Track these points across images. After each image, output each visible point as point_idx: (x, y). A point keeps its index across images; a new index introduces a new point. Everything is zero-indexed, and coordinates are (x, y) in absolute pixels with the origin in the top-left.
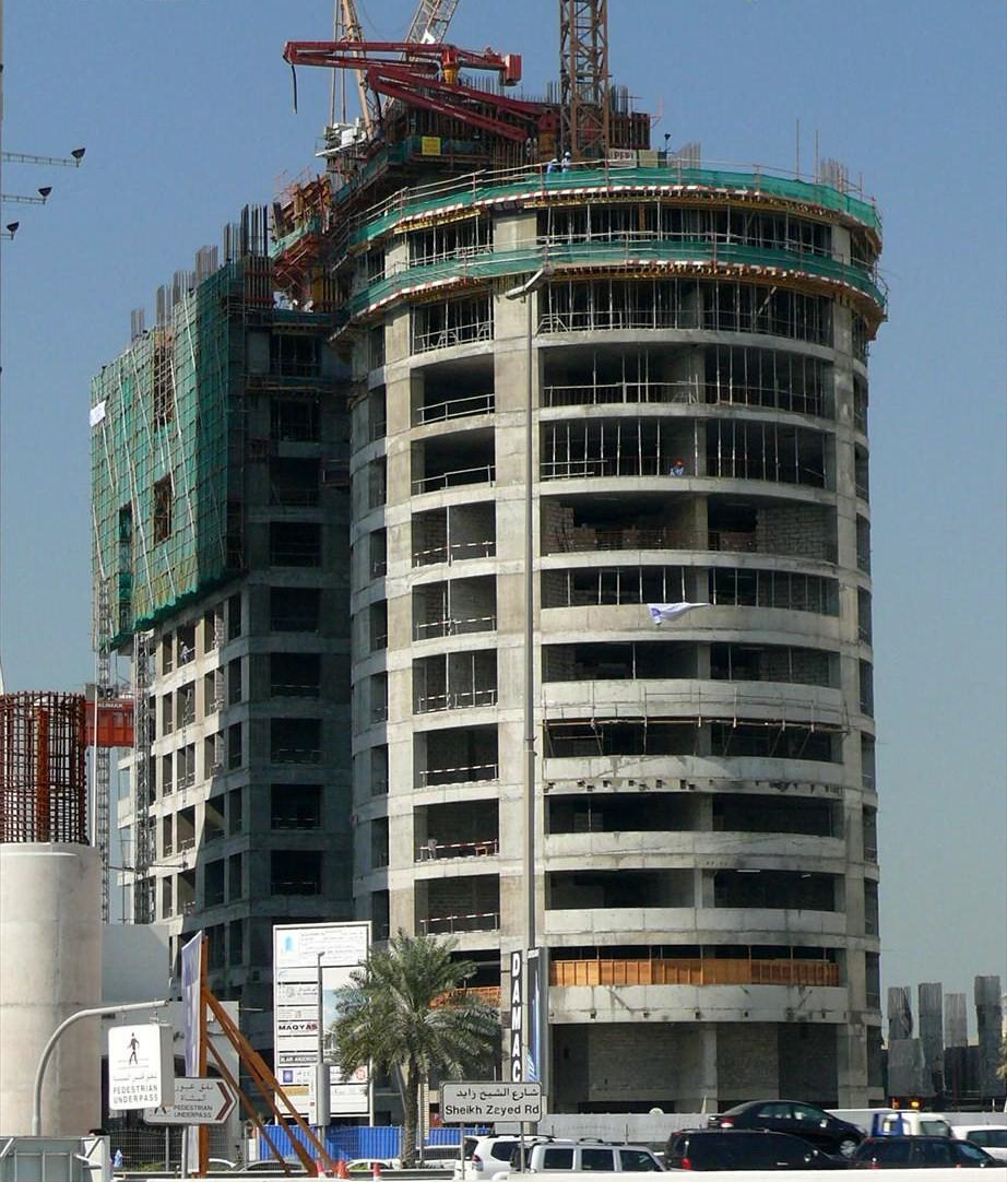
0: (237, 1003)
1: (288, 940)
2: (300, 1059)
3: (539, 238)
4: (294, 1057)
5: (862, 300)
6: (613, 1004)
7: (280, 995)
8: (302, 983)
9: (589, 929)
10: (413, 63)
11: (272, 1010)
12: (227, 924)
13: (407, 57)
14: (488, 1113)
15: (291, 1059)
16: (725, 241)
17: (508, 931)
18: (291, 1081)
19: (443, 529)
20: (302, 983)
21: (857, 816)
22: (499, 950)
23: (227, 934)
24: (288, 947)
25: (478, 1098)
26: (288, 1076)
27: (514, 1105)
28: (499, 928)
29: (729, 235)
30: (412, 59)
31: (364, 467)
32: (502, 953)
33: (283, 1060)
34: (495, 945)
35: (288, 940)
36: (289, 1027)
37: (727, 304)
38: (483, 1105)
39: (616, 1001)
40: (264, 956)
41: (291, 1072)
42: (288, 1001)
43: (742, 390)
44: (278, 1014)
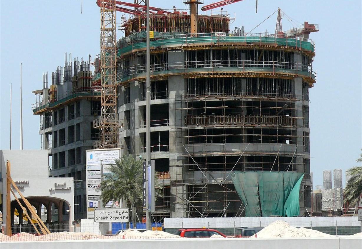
0: (73, 178)
1: (91, 155)
2: (95, 198)
4: (93, 198)
5: (305, 177)
6: (210, 178)
7: (88, 175)
8: (96, 171)
9: (201, 151)
11: (86, 180)
12: (76, 149)
14: (110, 219)
15: (92, 198)
17: (172, 151)
18: (92, 206)
20: (96, 171)
21: (301, 109)
22: (169, 158)
23: (76, 152)
24: (91, 158)
25: (107, 214)
26: (91, 204)
27: (120, 216)
28: (169, 150)
32: (170, 159)
33: (89, 198)
35: (91, 155)
37: (306, 71)
38: (109, 216)
39: (211, 177)
40: (82, 160)
41: (92, 203)
44: (88, 182)
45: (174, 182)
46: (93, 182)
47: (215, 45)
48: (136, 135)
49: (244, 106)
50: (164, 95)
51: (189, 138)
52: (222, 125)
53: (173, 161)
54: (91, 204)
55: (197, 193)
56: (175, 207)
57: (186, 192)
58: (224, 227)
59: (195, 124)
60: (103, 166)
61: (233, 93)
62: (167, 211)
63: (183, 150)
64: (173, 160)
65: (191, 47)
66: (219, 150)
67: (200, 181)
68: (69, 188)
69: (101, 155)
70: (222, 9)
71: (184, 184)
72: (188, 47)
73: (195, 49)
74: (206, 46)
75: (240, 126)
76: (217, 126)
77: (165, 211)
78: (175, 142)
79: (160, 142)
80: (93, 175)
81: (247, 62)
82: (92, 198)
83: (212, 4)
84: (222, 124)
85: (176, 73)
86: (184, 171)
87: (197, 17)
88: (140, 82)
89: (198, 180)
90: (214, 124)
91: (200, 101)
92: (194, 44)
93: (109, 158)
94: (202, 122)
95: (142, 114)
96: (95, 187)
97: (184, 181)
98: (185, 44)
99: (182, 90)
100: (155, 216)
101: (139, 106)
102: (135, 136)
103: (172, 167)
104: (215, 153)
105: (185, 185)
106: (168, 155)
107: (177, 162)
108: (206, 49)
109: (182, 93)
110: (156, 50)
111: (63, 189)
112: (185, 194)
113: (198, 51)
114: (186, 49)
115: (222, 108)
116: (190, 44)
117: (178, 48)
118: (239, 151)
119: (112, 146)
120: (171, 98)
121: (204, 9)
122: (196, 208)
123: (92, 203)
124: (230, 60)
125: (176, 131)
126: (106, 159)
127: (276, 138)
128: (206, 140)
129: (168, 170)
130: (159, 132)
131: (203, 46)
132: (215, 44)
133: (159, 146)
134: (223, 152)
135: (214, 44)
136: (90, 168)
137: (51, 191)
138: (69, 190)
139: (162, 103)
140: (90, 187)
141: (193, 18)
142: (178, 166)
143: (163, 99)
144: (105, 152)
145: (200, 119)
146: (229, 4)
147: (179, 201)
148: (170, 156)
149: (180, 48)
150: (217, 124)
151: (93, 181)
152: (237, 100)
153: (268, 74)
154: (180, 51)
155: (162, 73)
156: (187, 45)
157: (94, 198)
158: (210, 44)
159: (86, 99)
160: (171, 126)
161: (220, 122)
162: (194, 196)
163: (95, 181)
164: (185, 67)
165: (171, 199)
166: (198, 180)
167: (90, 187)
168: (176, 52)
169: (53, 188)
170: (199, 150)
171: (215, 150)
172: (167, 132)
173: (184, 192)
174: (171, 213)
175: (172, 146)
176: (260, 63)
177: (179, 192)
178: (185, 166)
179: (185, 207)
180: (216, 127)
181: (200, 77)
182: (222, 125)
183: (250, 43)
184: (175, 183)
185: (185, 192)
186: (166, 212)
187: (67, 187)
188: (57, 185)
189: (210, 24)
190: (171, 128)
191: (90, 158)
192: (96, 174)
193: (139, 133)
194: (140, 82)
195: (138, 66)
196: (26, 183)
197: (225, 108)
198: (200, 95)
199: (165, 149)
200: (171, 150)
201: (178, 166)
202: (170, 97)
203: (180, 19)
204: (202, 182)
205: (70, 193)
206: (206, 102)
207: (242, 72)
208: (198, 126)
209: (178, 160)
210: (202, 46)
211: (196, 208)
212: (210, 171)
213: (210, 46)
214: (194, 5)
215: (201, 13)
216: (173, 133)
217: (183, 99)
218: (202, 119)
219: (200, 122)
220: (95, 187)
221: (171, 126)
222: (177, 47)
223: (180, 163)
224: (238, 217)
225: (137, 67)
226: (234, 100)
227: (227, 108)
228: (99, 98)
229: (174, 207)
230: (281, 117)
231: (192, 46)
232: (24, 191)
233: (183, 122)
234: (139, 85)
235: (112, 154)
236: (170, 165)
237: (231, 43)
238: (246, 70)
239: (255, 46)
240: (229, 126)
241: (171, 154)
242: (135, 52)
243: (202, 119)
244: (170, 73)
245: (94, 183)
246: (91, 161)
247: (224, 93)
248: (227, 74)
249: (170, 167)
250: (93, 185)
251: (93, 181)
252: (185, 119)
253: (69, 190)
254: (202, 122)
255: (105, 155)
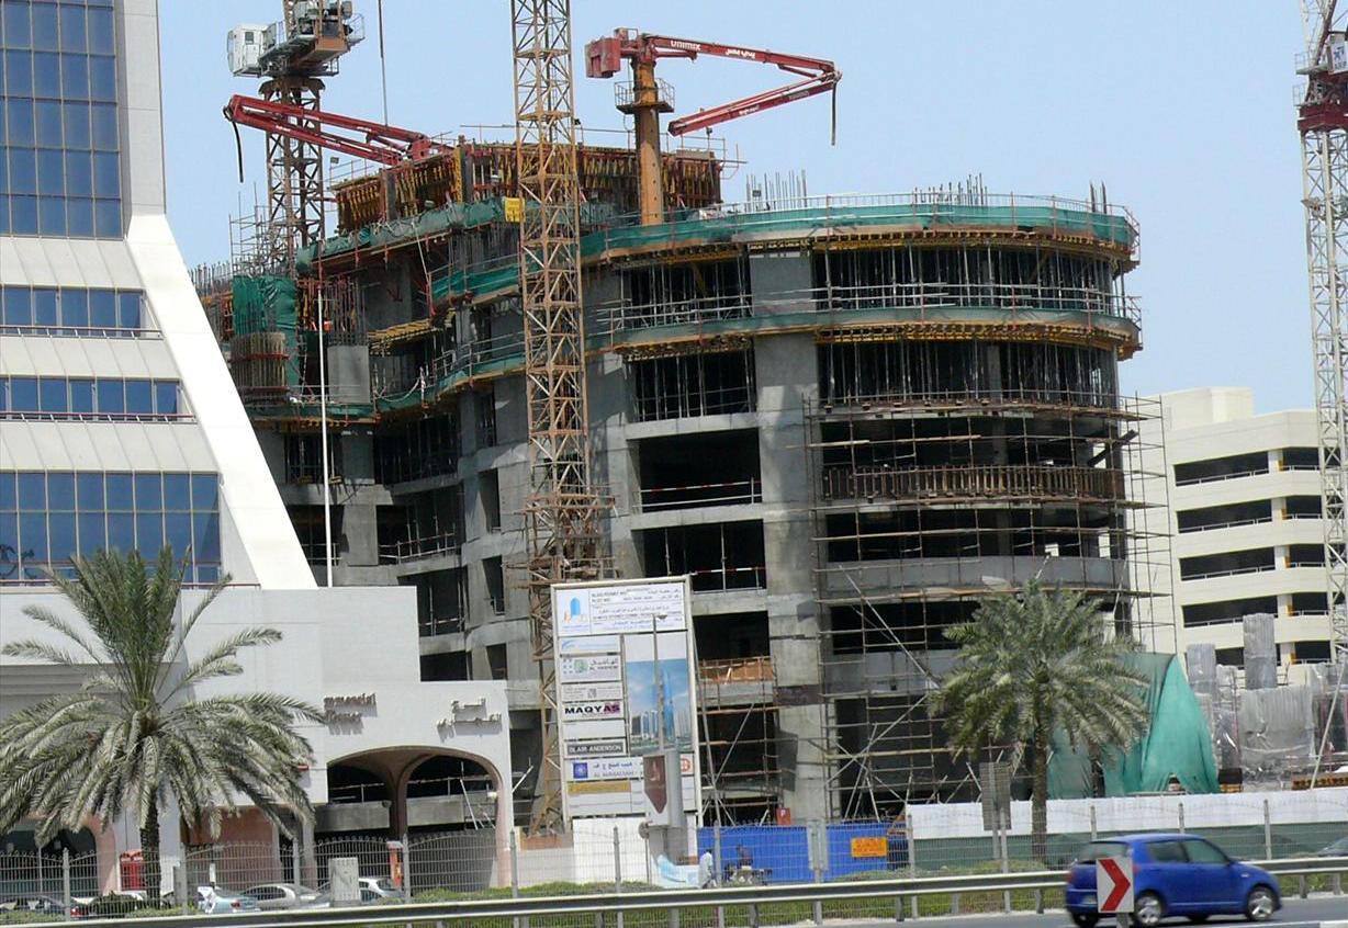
2: (597, 749)
3: (436, 644)
4: (588, 747)
9: (885, 584)
10: (373, 148)
13: (368, 139)
15: (585, 749)
16: (827, 307)
18: (586, 776)
19: (460, 922)
22: (766, 612)
29: (830, 288)
30: (374, 143)
31: (467, 455)
32: (769, 615)
33: (573, 750)
34: (761, 606)
36: (579, 709)
41: (586, 764)
42: (575, 677)
43: (971, 282)
45: (790, 691)
46: (585, 693)
47: (925, 232)
48: (613, 540)
49: (1028, 434)
50: (741, 400)
51: (981, 536)
52: (951, 496)
53: (782, 621)
54: (580, 770)
55: (895, 723)
56: (794, 775)
57: (838, 723)
58: (1070, 831)
59: (861, 495)
60: (625, 637)
61: (905, 394)
62: (764, 789)
63: (821, 584)
64: (782, 617)
65: (844, 239)
66: (945, 581)
67: (884, 686)
68: (495, 718)
69: (615, 599)
70: (709, 132)
71: (829, 698)
72: (833, 239)
73: (851, 248)
74: (897, 236)
75: (1002, 501)
76: (936, 500)
77: (759, 788)
78: (784, 560)
79: (723, 558)
80: (586, 670)
81: (927, 290)
82: (585, 749)
83: (699, 112)
84: (951, 494)
85: (791, 325)
86: (824, 655)
87: (660, 155)
88: (630, 360)
89: (879, 683)
90: (923, 493)
91: (873, 418)
92: (855, 229)
93: (647, 609)
94: (883, 489)
95: (636, 469)
96: (595, 710)
97: (827, 686)
98: (826, 229)
99: (807, 384)
100: (732, 808)
101: (627, 440)
102: (610, 542)
103: (778, 641)
104: (930, 591)
105: (832, 700)
106: (762, 601)
107: (798, 625)
108: (896, 247)
109: (810, 391)
110: (706, 249)
111: (478, 721)
112: (833, 728)
113: (861, 252)
114: (822, 246)
115: (948, 441)
116: (842, 228)
117: (790, 245)
118: (1004, 584)
119: (590, 573)
120: (768, 411)
121: (675, 129)
122: (878, 774)
123: (586, 764)
124: (833, 285)
125: (789, 522)
126: (634, 612)
127: (971, 538)
128: (978, 545)
129: (765, 650)
130: (719, 524)
131: (886, 237)
132: (925, 228)
133: (723, 570)
134: (955, 587)
135: (922, 229)
136: (573, 646)
137: (441, 727)
138: (494, 724)
139: (732, 428)
140: (573, 710)
141: (648, 159)
142: (801, 637)
143: (734, 415)
144: (629, 590)
145: (878, 479)
146: (749, 113)
147: (807, 753)
148: (770, 605)
149: (797, 245)
150: (935, 495)
151: (584, 689)
152: (990, 414)
153: (1055, 330)
154: (797, 254)
155: (738, 328)
156: (831, 234)
157: (591, 749)
158: (909, 230)
159: (274, 427)
160: (769, 503)
161: (945, 488)
162: (884, 736)
163: (594, 691)
164: (822, 306)
165: (777, 748)
166: (879, 683)
167: (573, 710)
168: (782, 255)
169: (451, 718)
170: (877, 583)
171: (928, 581)
172: (757, 526)
173: (827, 723)
174: (782, 797)
175: (773, 570)
176: (729, 303)
177: (809, 725)
178: (828, 636)
179: (836, 772)
180: (932, 504)
181: (870, 339)
182: (951, 496)
183: (1030, 229)
184: (799, 695)
185: (832, 723)
186: (762, 791)
187: (489, 714)
188: (461, 705)
189: (673, 183)
190: (770, 509)
191: (569, 614)
192: (596, 667)
193: (632, 531)
194: (630, 360)
195: (627, 304)
196: (368, 703)
197: (973, 440)
198: (935, 397)
199: (756, 579)
200: (775, 585)
201: (801, 637)
202: (761, 405)
203: (590, 160)
204: (894, 688)
205: (497, 733)
206: (916, 420)
207: (1010, 323)
208: (871, 501)
209: (801, 617)
210: (883, 236)
211: (878, 774)
212: (918, 652)
213: (908, 235)
214: (651, 114)
215: (670, 144)
216: (779, 528)
217: (814, 412)
218: (883, 480)
219: (879, 487)
220: (595, 710)
221: (769, 503)
222: (784, 241)
223: (810, 627)
224: (975, 801)
225: (622, 309)
226: (981, 414)
227: (979, 439)
228: (314, 423)
229: (793, 777)
230: (944, 470)
231: (849, 234)
232: (363, 731)
233: (820, 492)
234: (626, 372)
235: (655, 597)
236: (771, 634)
237: (972, 228)
238: (1021, 315)
239: (1041, 236)
240: (972, 503)
241: (771, 598)
242: (616, 259)
243: (883, 480)
244: (768, 327)
245: (589, 696)
246: (576, 620)
247: (911, 393)
248: (878, 331)
249: (771, 642)
250: (587, 705)
251: (584, 689)
252: (824, 481)
253: (494, 724)
254: (883, 489)
255: (630, 599)
